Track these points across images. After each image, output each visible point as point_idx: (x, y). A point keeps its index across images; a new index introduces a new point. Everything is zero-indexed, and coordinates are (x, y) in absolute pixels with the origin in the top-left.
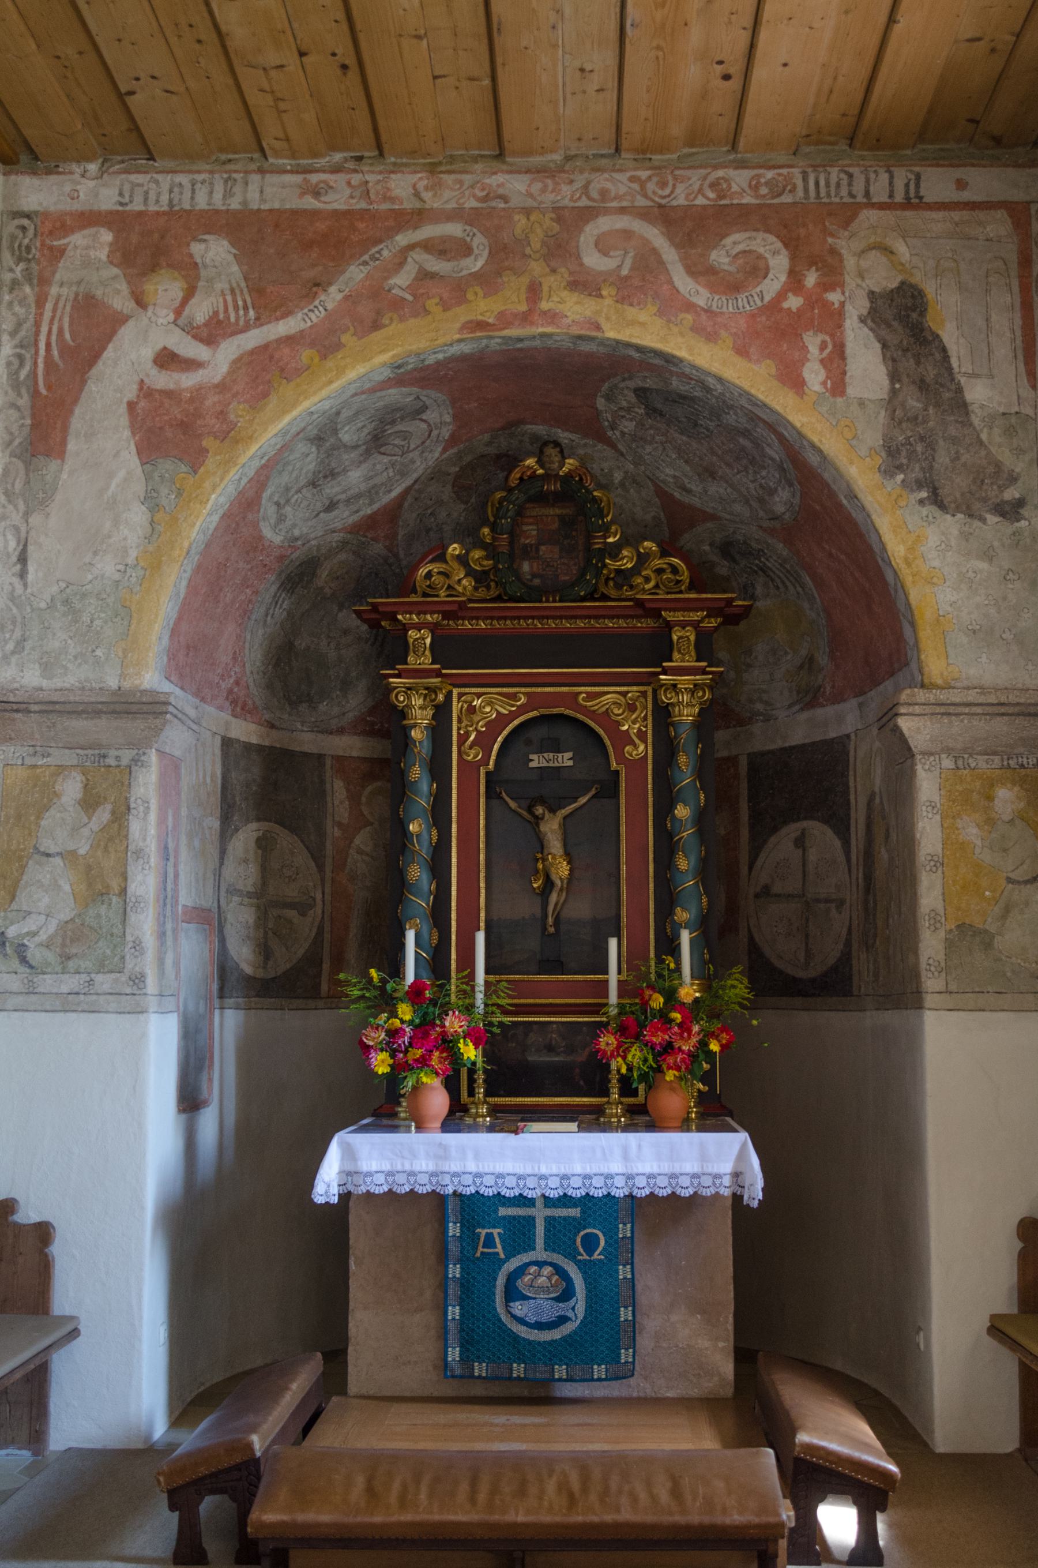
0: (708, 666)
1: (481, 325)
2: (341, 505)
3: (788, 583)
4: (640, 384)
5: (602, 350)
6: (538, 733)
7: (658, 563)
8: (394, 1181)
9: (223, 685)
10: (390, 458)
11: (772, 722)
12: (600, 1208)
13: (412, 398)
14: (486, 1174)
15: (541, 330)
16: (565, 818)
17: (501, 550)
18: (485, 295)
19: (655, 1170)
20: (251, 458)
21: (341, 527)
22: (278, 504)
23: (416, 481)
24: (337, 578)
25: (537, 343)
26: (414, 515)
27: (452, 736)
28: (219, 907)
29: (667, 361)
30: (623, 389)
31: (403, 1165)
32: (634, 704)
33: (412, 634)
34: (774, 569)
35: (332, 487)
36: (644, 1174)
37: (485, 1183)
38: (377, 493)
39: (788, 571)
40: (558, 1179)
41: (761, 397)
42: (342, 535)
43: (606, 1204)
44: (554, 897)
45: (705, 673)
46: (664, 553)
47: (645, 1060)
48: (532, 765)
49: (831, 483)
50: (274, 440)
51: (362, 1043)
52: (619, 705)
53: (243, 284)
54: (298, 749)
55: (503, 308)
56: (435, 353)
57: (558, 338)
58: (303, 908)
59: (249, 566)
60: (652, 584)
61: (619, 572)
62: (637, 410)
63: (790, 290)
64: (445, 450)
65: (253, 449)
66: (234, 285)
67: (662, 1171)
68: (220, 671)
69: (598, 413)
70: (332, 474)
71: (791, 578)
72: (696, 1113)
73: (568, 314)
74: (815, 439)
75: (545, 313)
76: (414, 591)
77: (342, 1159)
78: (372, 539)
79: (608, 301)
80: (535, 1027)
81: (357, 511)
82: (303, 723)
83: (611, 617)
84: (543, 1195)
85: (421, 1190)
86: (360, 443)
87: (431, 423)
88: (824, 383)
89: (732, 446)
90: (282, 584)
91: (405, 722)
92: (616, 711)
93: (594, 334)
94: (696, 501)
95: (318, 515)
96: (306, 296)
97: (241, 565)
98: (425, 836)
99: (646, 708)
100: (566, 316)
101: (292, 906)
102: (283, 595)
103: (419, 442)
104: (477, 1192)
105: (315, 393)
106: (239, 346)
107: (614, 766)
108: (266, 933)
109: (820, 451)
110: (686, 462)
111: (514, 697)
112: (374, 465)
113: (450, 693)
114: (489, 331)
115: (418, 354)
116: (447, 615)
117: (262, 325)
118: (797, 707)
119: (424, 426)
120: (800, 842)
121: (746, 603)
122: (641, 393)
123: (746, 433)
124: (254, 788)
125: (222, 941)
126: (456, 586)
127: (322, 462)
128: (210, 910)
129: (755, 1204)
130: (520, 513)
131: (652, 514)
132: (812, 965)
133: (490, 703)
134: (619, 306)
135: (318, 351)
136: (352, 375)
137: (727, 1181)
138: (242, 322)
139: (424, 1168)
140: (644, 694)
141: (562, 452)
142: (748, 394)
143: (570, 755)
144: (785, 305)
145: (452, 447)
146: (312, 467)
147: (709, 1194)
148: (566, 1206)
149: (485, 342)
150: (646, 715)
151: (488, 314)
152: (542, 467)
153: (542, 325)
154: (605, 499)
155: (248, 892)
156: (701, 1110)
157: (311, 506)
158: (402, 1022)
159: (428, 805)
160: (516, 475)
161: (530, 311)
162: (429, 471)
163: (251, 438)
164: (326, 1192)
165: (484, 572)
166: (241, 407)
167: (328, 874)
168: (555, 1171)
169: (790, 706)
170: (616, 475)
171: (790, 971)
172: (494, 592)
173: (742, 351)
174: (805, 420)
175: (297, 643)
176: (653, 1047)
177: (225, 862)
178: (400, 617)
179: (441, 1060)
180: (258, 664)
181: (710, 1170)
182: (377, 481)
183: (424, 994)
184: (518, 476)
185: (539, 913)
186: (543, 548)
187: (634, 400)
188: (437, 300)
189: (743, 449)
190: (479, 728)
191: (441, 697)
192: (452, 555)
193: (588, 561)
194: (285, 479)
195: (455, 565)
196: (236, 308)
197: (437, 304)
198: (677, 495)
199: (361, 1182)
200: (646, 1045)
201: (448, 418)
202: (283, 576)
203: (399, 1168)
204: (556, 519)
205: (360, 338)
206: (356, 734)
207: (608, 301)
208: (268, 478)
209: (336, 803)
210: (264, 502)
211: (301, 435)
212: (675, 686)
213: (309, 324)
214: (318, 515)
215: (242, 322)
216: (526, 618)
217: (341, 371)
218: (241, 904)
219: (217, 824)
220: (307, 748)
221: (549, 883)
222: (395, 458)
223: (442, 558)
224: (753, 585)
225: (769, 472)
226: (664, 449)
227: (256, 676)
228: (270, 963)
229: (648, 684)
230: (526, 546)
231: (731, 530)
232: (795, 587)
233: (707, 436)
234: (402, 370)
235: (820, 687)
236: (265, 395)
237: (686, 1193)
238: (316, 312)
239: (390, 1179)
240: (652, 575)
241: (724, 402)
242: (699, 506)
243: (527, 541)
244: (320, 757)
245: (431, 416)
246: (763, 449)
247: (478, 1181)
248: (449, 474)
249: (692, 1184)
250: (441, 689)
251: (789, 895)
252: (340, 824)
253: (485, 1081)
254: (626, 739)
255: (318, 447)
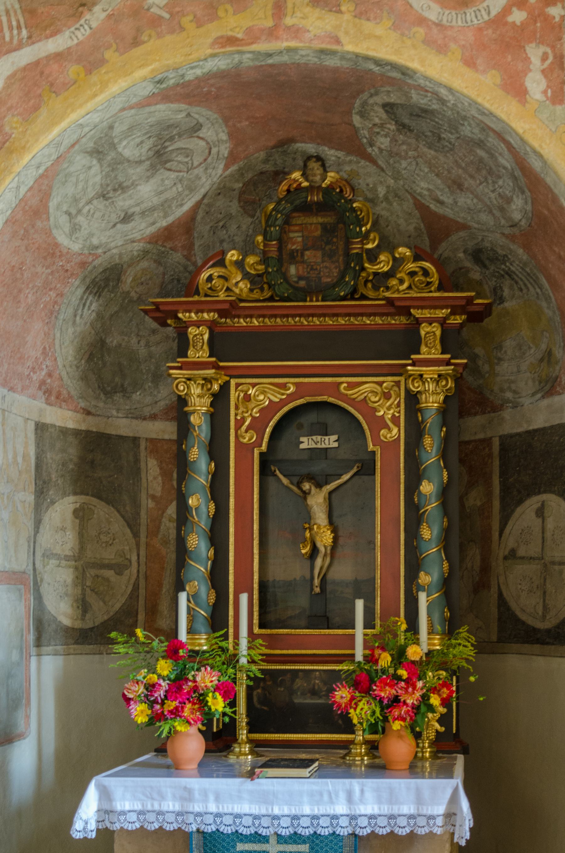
0: (452, 358)
1: (231, 41)
2: (136, 218)
3: (529, 285)
4: (387, 99)
5: (345, 64)
6: (312, 417)
7: (411, 266)
8: (145, 819)
9: (35, 378)
10: (177, 174)
11: (519, 408)
12: (327, 845)
13: (183, 114)
14: (226, 814)
15: (285, 44)
16: (330, 493)
17: (270, 255)
18: (234, 11)
19: (376, 811)
20: (26, 167)
21: (139, 237)
22: (69, 214)
23: (204, 196)
24: (142, 284)
25: (285, 58)
26: (208, 227)
27: (229, 421)
28: (35, 569)
29: (403, 74)
30: (372, 105)
31: (152, 805)
32: (389, 392)
33: (192, 331)
34: (517, 272)
35: (124, 200)
36: (366, 816)
37: (224, 822)
38: (170, 207)
39: (528, 274)
40: (289, 819)
41: (487, 105)
42: (141, 244)
43: (331, 841)
44: (319, 562)
45: (448, 363)
46: (417, 258)
47: (374, 713)
48: (302, 446)
49: (552, 187)
50: (46, 151)
51: (124, 695)
52: (375, 393)
53: (17, 6)
54: (114, 433)
55: (251, 24)
56: (192, 68)
57: (303, 53)
58: (119, 569)
59: (49, 271)
60: (406, 285)
61: (376, 274)
62: (388, 126)
63: (514, 5)
64: (226, 167)
65: (27, 158)
66: (9, 7)
67: (382, 813)
68: (29, 363)
69: (356, 130)
70: (121, 188)
71: (532, 281)
72: (430, 752)
73: (311, 29)
74: (536, 144)
75: (289, 28)
76: (197, 293)
77: (100, 799)
78: (171, 249)
79: (347, 17)
80: (300, 673)
81: (153, 223)
82: (118, 410)
83: (369, 315)
84: (276, 833)
85: (168, 827)
86: (143, 158)
87: (209, 140)
88: (545, 92)
89: (472, 158)
90: (87, 288)
91: (186, 409)
92: (373, 399)
93: (334, 47)
94: (448, 212)
95: (114, 225)
96: (73, 15)
97: (39, 269)
98: (203, 509)
99: (399, 395)
100: (308, 31)
101: (109, 567)
102: (91, 298)
103: (201, 160)
104: (218, 830)
105: (81, 106)
106: (13, 63)
107: (371, 447)
108: (83, 590)
109: (540, 156)
110: (437, 175)
111: (284, 386)
112: (163, 180)
113: (227, 384)
114: (238, 46)
115: (176, 69)
116: (223, 313)
117: (33, 43)
118: (539, 396)
119: (202, 143)
120: (540, 512)
121: (486, 301)
122: (388, 107)
123: (480, 144)
124: (71, 467)
125: (39, 598)
126: (234, 289)
127: (107, 176)
128: (24, 573)
129: (463, 843)
130: (287, 222)
131: (414, 225)
132: (548, 618)
133: (263, 392)
134: (357, 20)
135: (84, 66)
136: (115, 88)
137: (440, 821)
138: (15, 41)
139: (171, 808)
140: (398, 384)
141: (323, 166)
142: (476, 103)
143: (335, 437)
144: (510, 19)
145: (233, 164)
146: (98, 179)
147: (423, 833)
148: (295, 842)
149: (237, 57)
150: (399, 402)
151: (238, 29)
152: (307, 180)
153: (287, 40)
154: (365, 209)
155: (66, 556)
156: (435, 750)
157: (106, 217)
158: (159, 676)
159: (207, 482)
160: (284, 187)
161: (276, 26)
162: (215, 186)
163: (24, 148)
164: (84, 829)
165: (259, 275)
166: (15, 119)
167: (143, 539)
168: (286, 811)
169: (533, 395)
170: (379, 189)
171: (530, 621)
172: (267, 294)
173: (470, 63)
174: (527, 126)
175: (108, 341)
176: (381, 700)
177: (41, 530)
178: (180, 315)
179: (192, 711)
180: (70, 358)
181: (424, 812)
182: (168, 195)
183: (178, 653)
184: (285, 188)
185: (308, 576)
186: (307, 253)
187: (384, 116)
188: (190, 17)
189: (481, 160)
190: (254, 414)
191: (216, 387)
192: (231, 261)
193: (347, 264)
194: (70, 190)
195: (233, 269)
196: (11, 28)
197: (191, 21)
198: (432, 207)
199: (116, 820)
200: (375, 699)
201: (224, 136)
202: (88, 281)
203: (149, 808)
204: (319, 227)
205: (122, 54)
206: (167, 420)
207: (347, 17)
208: (51, 188)
209: (150, 478)
210: (51, 211)
211: (77, 147)
212: (421, 376)
213: (76, 41)
214: (114, 225)
215: (15, 41)
216: (294, 316)
217: (104, 85)
218: (59, 566)
219: (31, 498)
220: (124, 432)
221: (314, 551)
222: (181, 174)
223: (221, 263)
224: (501, 288)
225: (504, 181)
226: (417, 164)
227: (69, 369)
228: (88, 616)
229: (400, 375)
230: (293, 251)
231: (480, 238)
232: (535, 289)
233: (451, 150)
234: (164, 86)
235: (557, 377)
236: (36, 108)
237: (402, 832)
238: (82, 30)
239: (142, 817)
240: (406, 278)
241: (458, 113)
242: (451, 216)
243: (294, 247)
244: (135, 440)
245: (207, 133)
246: (496, 159)
247: (218, 820)
248: (234, 190)
249: (409, 824)
250: (217, 380)
251: (531, 558)
252: (153, 497)
253: (248, 724)
254: (382, 423)
255: (100, 160)
